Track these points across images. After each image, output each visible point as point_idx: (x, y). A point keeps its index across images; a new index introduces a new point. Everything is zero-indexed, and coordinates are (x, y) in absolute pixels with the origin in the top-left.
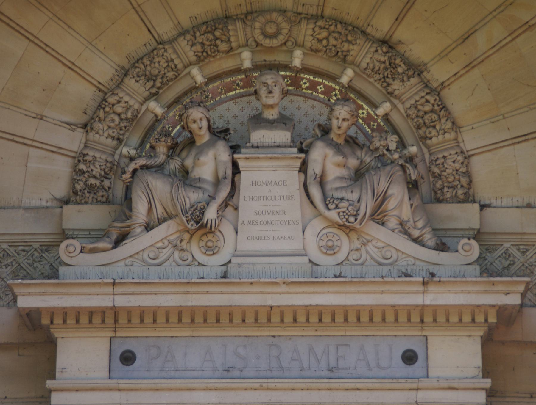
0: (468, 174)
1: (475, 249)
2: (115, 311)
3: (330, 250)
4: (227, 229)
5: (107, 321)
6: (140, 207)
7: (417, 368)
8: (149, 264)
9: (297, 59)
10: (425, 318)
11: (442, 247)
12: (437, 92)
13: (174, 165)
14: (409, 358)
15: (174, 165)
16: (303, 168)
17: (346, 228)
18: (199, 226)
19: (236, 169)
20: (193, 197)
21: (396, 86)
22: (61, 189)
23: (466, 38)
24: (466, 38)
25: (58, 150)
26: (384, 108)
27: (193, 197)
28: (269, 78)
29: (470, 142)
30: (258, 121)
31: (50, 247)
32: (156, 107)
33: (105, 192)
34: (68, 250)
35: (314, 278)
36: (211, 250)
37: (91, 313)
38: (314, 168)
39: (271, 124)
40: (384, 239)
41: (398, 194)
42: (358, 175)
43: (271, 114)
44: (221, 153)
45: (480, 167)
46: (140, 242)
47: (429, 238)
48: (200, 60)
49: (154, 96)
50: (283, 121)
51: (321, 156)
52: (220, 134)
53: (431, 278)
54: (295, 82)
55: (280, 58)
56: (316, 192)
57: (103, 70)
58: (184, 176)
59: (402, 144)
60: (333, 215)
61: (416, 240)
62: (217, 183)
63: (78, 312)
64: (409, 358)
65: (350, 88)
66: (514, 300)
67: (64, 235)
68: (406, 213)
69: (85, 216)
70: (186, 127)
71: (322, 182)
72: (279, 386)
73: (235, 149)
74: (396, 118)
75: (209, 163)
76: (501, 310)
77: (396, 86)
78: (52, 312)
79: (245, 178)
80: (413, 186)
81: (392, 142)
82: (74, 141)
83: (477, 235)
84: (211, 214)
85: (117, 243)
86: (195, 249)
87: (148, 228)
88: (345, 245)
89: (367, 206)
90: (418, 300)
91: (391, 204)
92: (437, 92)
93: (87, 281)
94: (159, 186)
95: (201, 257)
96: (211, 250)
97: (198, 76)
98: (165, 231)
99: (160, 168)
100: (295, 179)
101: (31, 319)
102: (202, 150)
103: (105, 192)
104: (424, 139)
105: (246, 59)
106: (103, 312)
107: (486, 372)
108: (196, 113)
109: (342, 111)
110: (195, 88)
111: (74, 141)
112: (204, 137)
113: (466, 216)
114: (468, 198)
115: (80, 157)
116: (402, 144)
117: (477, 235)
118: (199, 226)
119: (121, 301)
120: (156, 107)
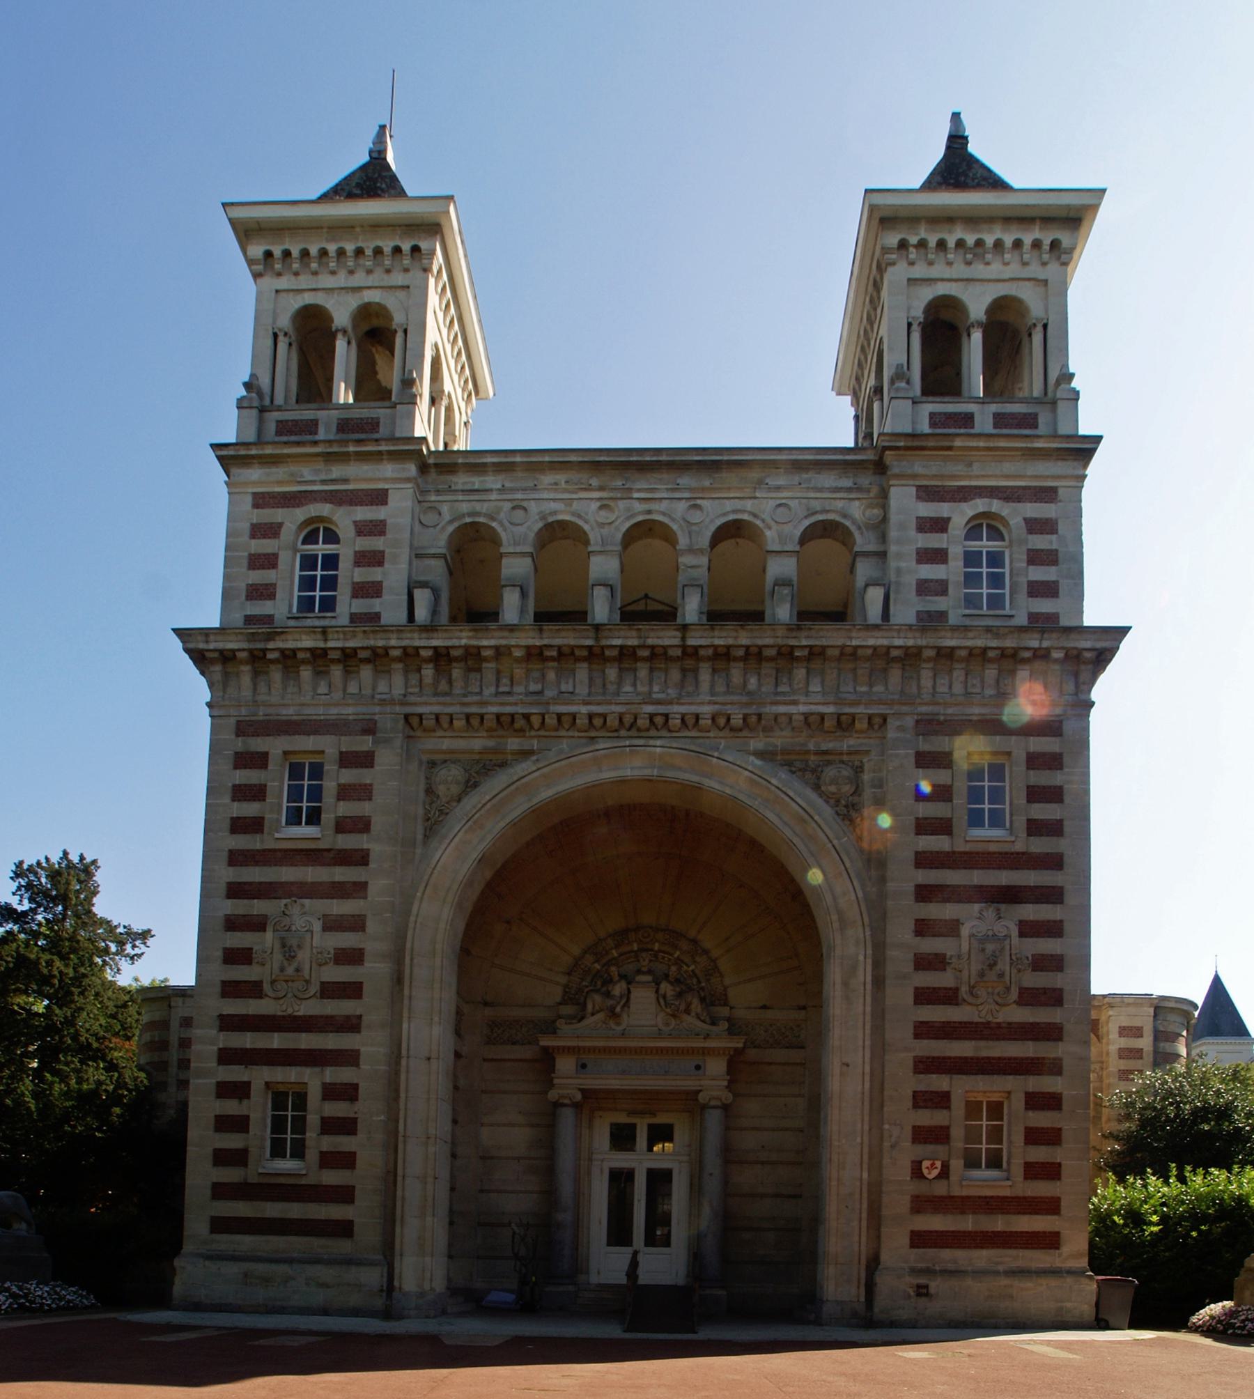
0: (726, 995)
1: (726, 1025)
2: (579, 1048)
3: (667, 1024)
4: (625, 1016)
5: (273, 691)
6: (590, 1006)
7: (700, 1072)
8: (591, 1030)
9: (656, 947)
10: (705, 1052)
11: (713, 1024)
12: (714, 961)
13: (604, 989)
14: (698, 1067)
15: (604, 989)
16: (657, 992)
17: (674, 1016)
18: (613, 1014)
19: (629, 992)
20: (611, 1002)
21: (698, 959)
22: (558, 999)
23: (727, 939)
24: (727, 939)
25: (558, 983)
26: (692, 967)
27: (611, 1002)
28: (644, 955)
29: (727, 981)
30: (639, 972)
31: (554, 1022)
32: (597, 966)
33: (575, 999)
34: (560, 1024)
35: (660, 1035)
36: (618, 1024)
37: (569, 1048)
38: (662, 991)
39: (644, 973)
40: (689, 1020)
41: (696, 1002)
42: (679, 995)
43: (645, 969)
44: (623, 984)
45: (732, 993)
46: (589, 1021)
47: (708, 1020)
48: (616, 947)
49: (597, 961)
50: (649, 972)
51: (665, 987)
52: (622, 977)
53: (707, 1037)
54: (656, 956)
55: (649, 946)
56: (662, 1001)
57: (576, 950)
58: (608, 995)
59: (699, 982)
60: (668, 1010)
61: (704, 1021)
62: (621, 997)
63: (564, 1048)
64: (698, 1067)
65: (678, 958)
66: (741, 1045)
67: (560, 1017)
68: (699, 1010)
69: (567, 1010)
70: (830, 637)
71: (664, 997)
72: (1034, 1265)
73: (629, 983)
74: (697, 972)
75: (618, 989)
76: (736, 1049)
77: (698, 959)
78: (554, 1048)
79: (632, 996)
80: (702, 1000)
81: (695, 981)
82: (563, 980)
83: (729, 1020)
84: (618, 1009)
85: (580, 1021)
86: (612, 1024)
87: (593, 1014)
88: (673, 1022)
89: (683, 1007)
90: (702, 1045)
91: (693, 1006)
92: (714, 961)
93: (568, 1035)
94: (598, 998)
95: (614, 1027)
96: (618, 1024)
97: (615, 953)
98: (600, 1016)
99: (597, 991)
100: (653, 996)
101: (545, 1050)
102: (616, 983)
103: (575, 999)
104: (708, 980)
105: (635, 947)
106: (574, 1048)
107: (728, 1073)
108: (613, 968)
109: (674, 968)
110: (614, 959)
111: (563, 980)
112: (616, 978)
113: (724, 1011)
114: (726, 1004)
115: (566, 986)
116: (699, 982)
117: (729, 1020)
118: (613, 1014)
119: (581, 1044)
120: (597, 966)
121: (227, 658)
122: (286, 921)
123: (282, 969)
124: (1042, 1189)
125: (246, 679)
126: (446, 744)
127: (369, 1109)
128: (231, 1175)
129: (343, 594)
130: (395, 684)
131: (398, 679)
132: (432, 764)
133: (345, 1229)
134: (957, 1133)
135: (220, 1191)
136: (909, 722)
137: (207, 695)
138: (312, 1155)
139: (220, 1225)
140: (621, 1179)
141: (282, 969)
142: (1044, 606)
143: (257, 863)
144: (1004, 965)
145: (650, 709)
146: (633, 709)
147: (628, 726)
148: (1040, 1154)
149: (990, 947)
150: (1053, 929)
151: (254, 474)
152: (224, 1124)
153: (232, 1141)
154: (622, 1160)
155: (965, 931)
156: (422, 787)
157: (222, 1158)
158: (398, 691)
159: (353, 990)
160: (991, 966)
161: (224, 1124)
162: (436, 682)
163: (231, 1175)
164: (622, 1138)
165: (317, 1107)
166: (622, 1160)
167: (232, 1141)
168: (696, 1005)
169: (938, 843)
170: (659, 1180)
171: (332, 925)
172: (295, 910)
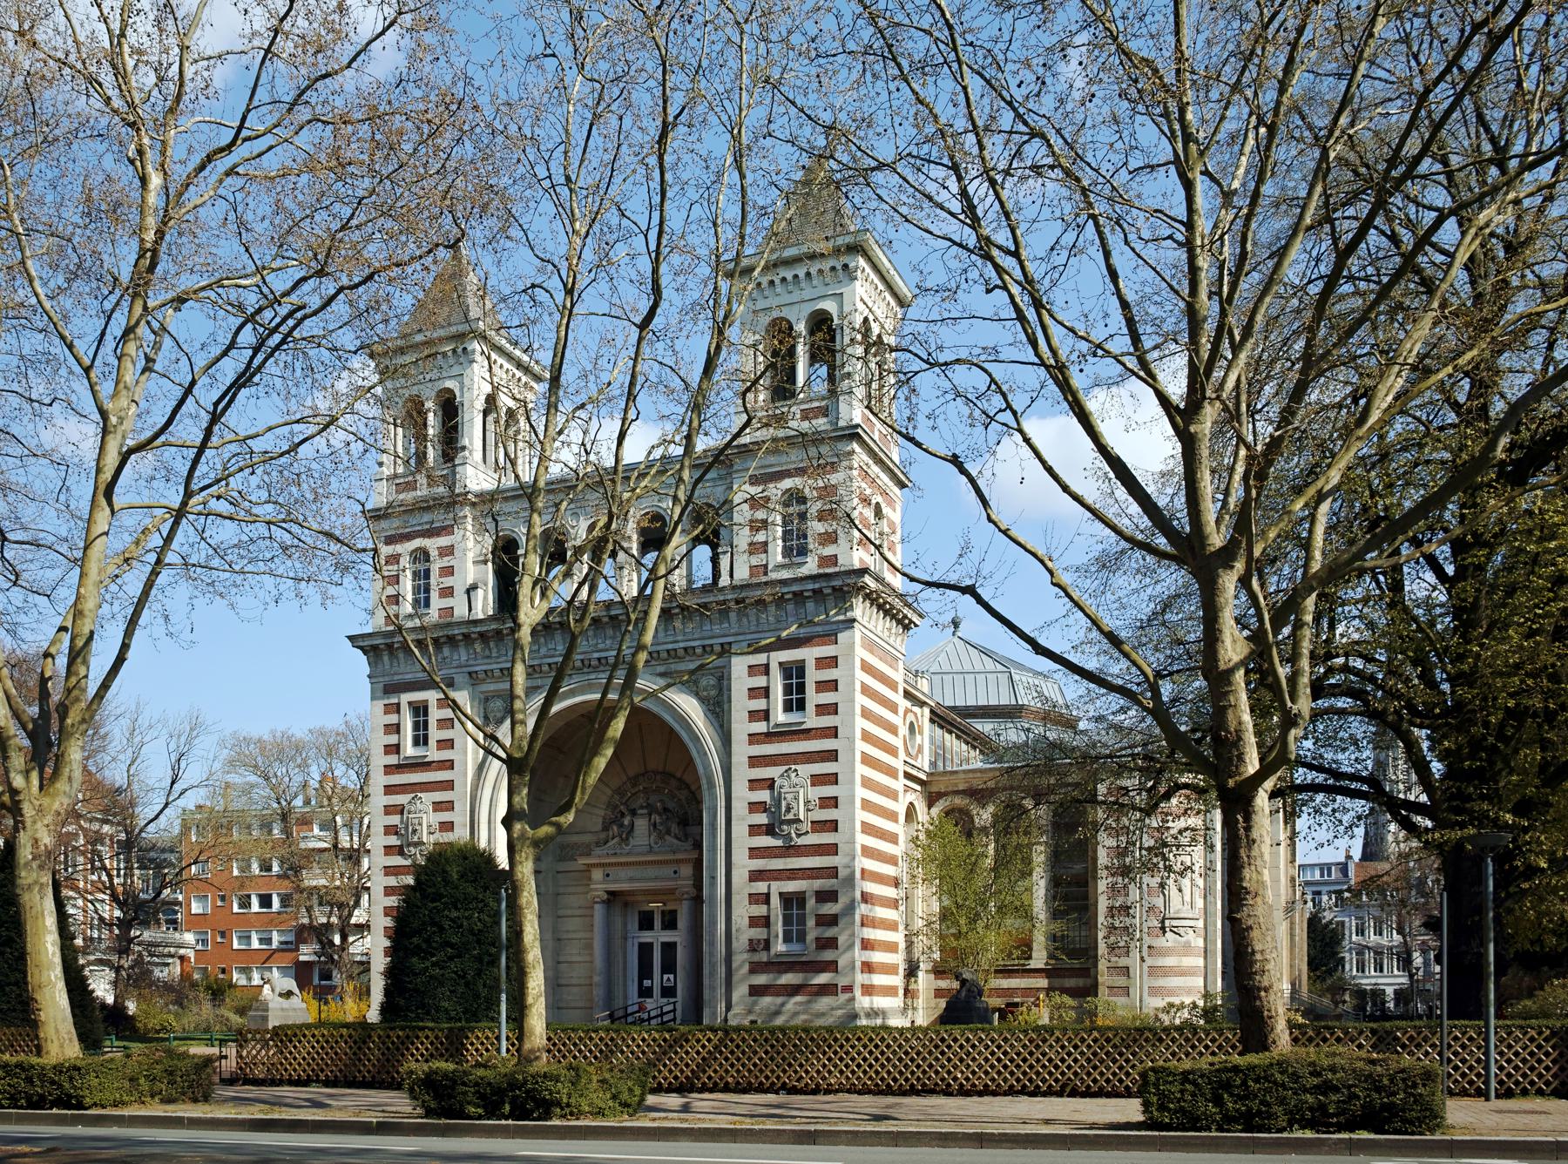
10: (678, 861)
121: (375, 648)
125: (386, 658)
126: (492, 687)
128: (761, 727)
129: (434, 595)
130: (463, 655)
131: (462, 651)
132: (487, 700)
134: (811, 923)
137: (367, 670)
140: (646, 949)
142: (828, 551)
145: (596, 655)
150: (833, 779)
151: (384, 524)
152: (754, 693)
154: (647, 937)
157: (754, 716)
158: (464, 658)
161: (754, 693)
162: (483, 650)
163: (761, 727)
164: (646, 922)
165: (812, 676)
166: (647, 937)
168: (674, 828)
170: (669, 948)
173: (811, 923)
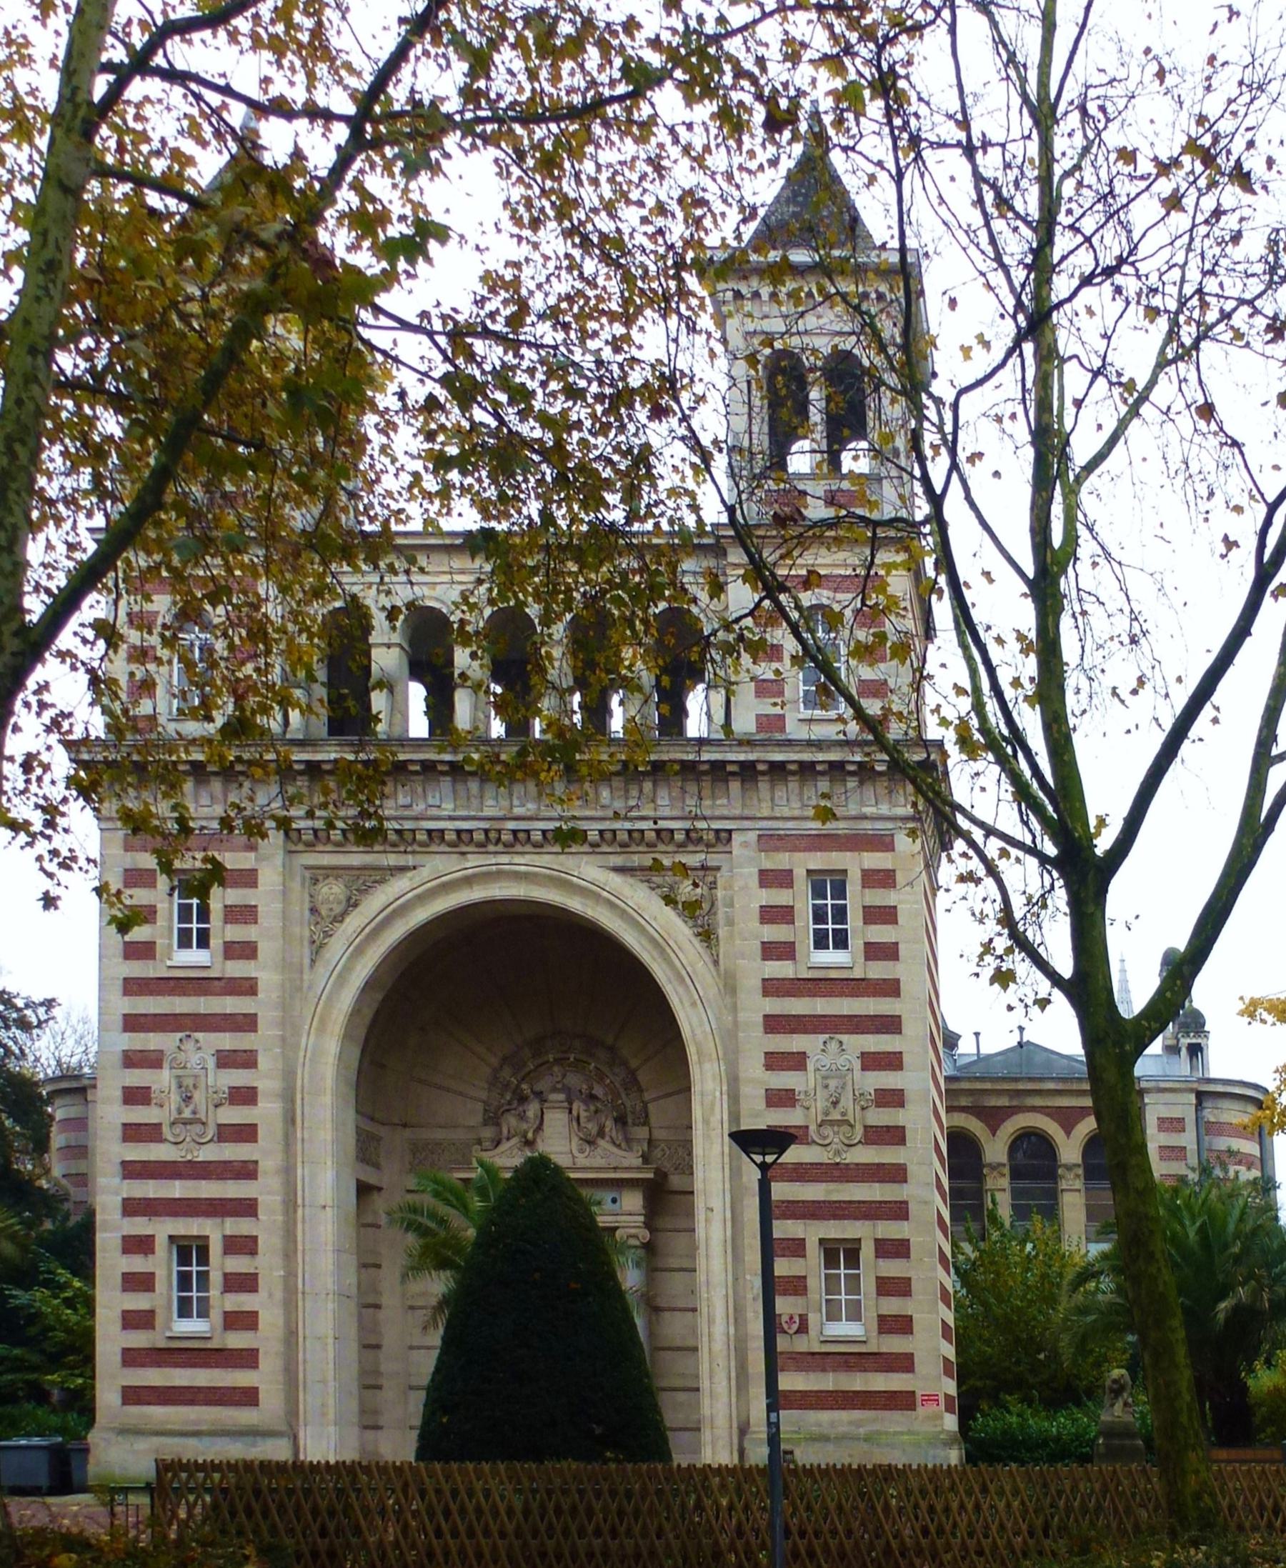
46: (505, 1146)
75: (532, 1109)
89: (594, 1131)
122: (181, 1057)
123: (180, 1112)
124: (894, 1344)
127: (267, 1264)
133: (249, 1397)
134: (868, 1284)
135: (131, 1358)
136: (753, 836)
138: (216, 1315)
139: (132, 1395)
141: (180, 1112)
143: (151, 993)
144: (847, 1102)
145: (511, 825)
146: (497, 825)
147: (490, 840)
148: (892, 1306)
149: (833, 1083)
153: (139, 1302)
155: (810, 1066)
156: (307, 906)
159: (246, 1133)
160: (835, 1104)
167: (139, 1302)
169: (782, 969)
171: (226, 1060)
172: (189, 1045)
173: (868, 1284)
